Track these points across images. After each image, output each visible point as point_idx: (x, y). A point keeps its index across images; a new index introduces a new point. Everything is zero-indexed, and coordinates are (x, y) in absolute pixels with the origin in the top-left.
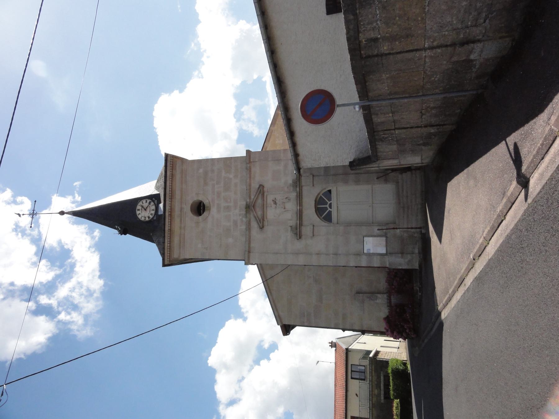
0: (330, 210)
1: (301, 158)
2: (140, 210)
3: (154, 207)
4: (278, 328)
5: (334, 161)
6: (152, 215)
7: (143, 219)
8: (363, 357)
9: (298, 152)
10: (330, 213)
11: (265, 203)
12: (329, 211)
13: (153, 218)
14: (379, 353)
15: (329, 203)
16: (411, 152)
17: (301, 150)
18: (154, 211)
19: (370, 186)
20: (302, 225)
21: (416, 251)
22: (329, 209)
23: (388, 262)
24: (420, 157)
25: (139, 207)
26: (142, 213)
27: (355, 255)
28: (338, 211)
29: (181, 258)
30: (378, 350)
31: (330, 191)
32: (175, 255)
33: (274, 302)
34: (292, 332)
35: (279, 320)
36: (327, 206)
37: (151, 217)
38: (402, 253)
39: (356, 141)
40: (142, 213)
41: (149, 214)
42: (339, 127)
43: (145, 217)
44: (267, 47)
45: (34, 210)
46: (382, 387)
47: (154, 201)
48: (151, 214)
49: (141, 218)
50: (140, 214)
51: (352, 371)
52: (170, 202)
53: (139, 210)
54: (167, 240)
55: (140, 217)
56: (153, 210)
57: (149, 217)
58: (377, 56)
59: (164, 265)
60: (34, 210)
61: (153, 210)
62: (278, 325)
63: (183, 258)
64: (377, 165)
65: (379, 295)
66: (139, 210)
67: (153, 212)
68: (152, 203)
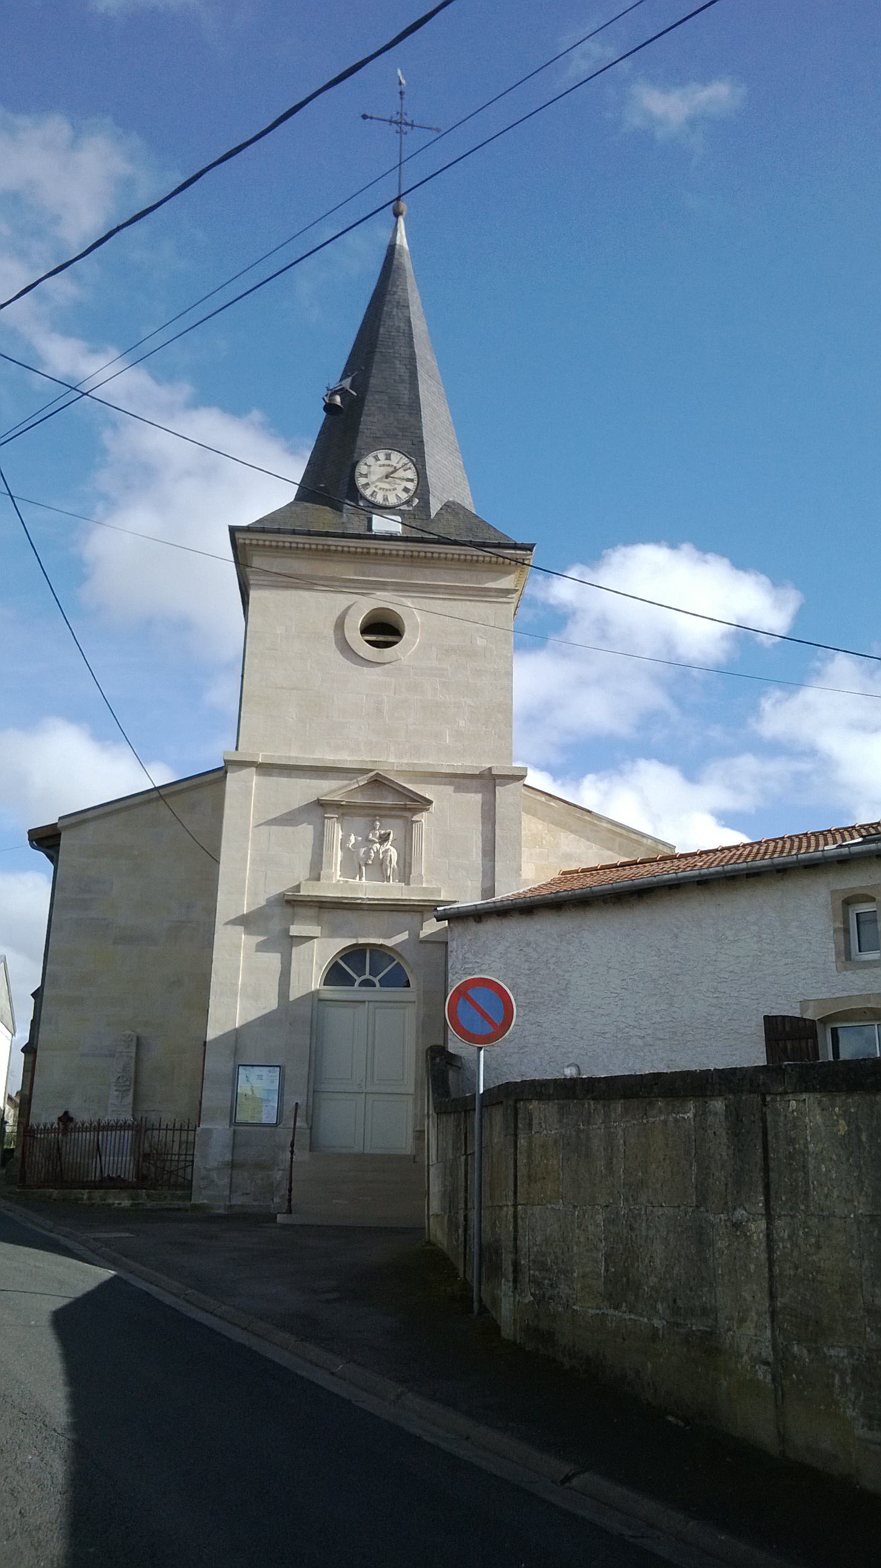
0: (357, 984)
1: (473, 926)
2: (388, 462)
3: (392, 501)
4: (50, 818)
6: (372, 495)
7: (362, 468)
10: (350, 982)
11: (383, 813)
13: (363, 498)
15: (376, 980)
18: (384, 500)
19: (412, 1090)
20: (320, 908)
21: (238, 1200)
22: (359, 980)
23: (217, 1128)
25: (397, 459)
27: (236, 1041)
28: (347, 1003)
29: (251, 577)
31: (408, 985)
32: (258, 562)
33: (127, 808)
34: (41, 855)
35: (73, 820)
36: (367, 976)
37: (367, 493)
38: (233, 1165)
39: (499, 1065)
42: (533, 1024)
45: (412, 126)
47: (408, 502)
48: (374, 491)
49: (366, 464)
52: (401, 553)
53: (388, 457)
55: (370, 460)
56: (386, 499)
58: (516, 1127)
60: (412, 126)
61: (386, 499)
62: (60, 818)
63: (251, 582)
66: (388, 457)
67: (379, 499)
68: (404, 496)
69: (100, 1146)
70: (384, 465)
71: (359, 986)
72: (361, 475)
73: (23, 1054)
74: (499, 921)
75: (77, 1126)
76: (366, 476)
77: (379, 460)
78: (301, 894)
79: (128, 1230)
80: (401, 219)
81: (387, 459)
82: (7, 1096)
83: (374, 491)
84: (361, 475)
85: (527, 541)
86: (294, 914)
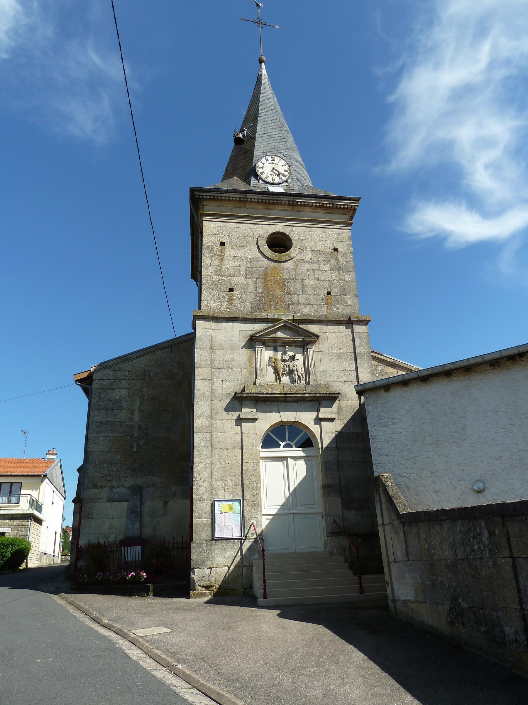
1: (383, 394)
2: (273, 162)
5: (380, 449)
8: (33, 500)
9: (391, 389)
12: (292, 442)
14: (38, 523)
15: (293, 444)
16: (428, 583)
17: (396, 394)
22: (283, 444)
24: (412, 599)
26: (269, 163)
30: (43, 522)
40: (269, 163)
41: (268, 173)
43: (262, 168)
44: (28, 477)
46: (122, 556)
49: (261, 163)
50: (268, 160)
51: (12, 484)
54: (231, 196)
57: (262, 173)
59: (193, 191)
64: (386, 521)
65: (137, 525)
69: (126, 557)
70: (271, 163)
71: (283, 447)
72: (259, 168)
73: (73, 504)
74: (404, 389)
75: (111, 544)
76: (262, 168)
77: (268, 161)
78: (245, 392)
79: (160, 624)
80: (263, 64)
81: (272, 160)
82: (62, 529)
83: (267, 176)
84: (259, 168)
85: (356, 196)
86: (241, 405)
